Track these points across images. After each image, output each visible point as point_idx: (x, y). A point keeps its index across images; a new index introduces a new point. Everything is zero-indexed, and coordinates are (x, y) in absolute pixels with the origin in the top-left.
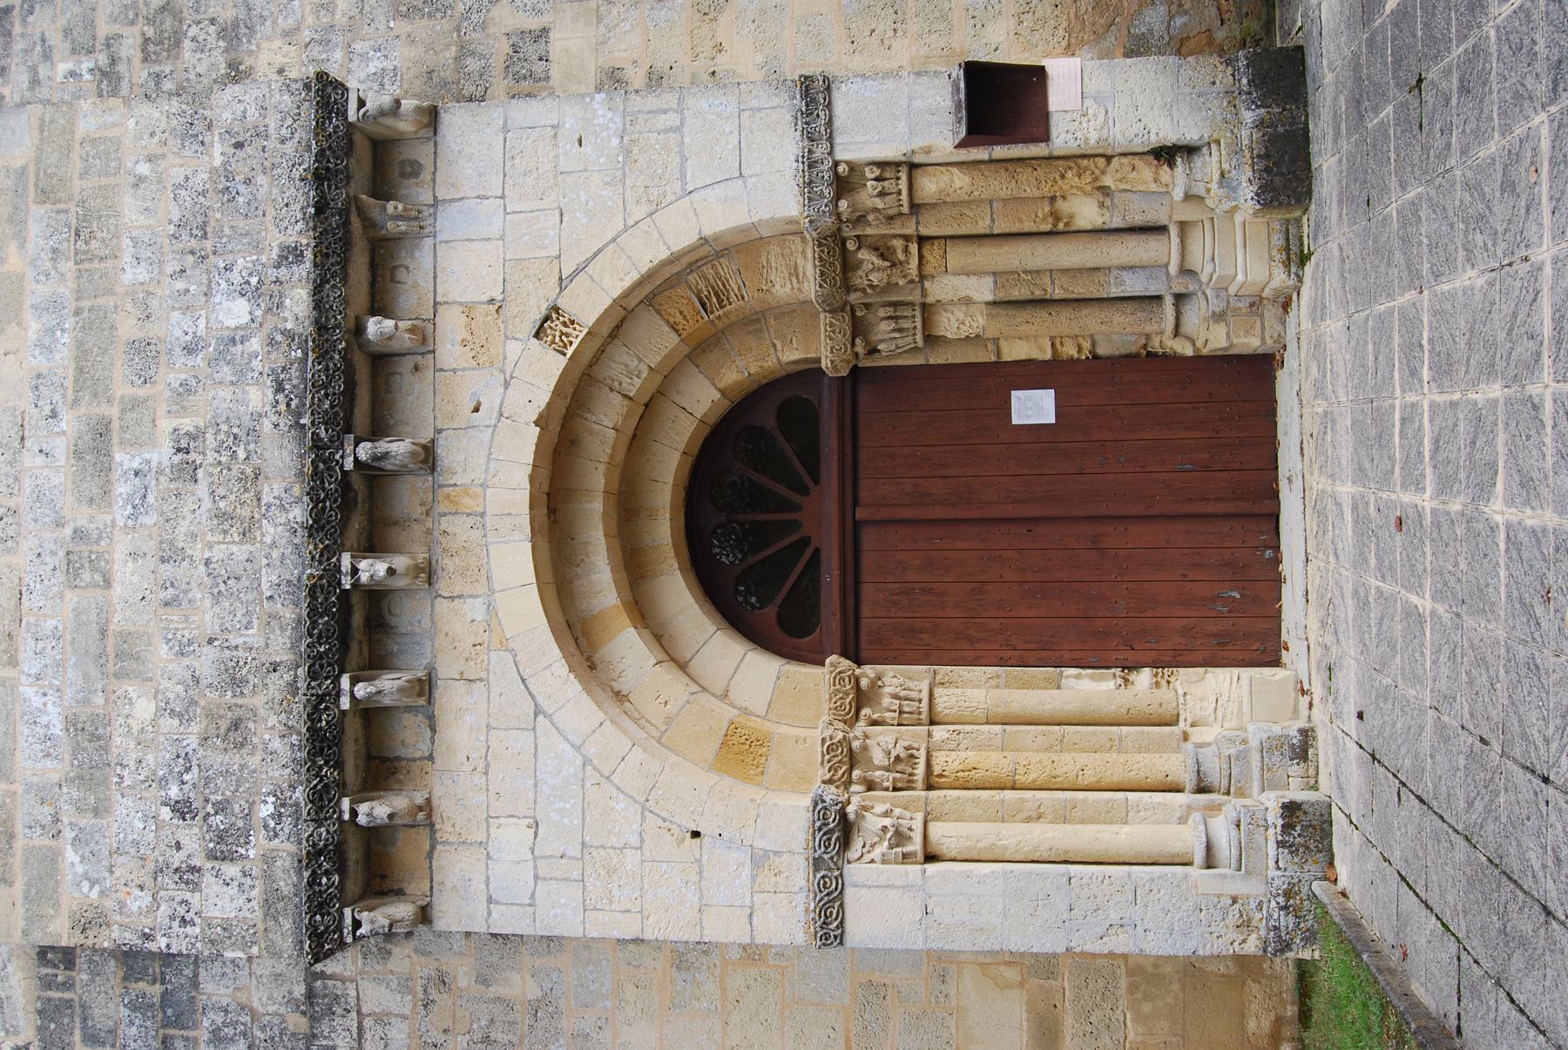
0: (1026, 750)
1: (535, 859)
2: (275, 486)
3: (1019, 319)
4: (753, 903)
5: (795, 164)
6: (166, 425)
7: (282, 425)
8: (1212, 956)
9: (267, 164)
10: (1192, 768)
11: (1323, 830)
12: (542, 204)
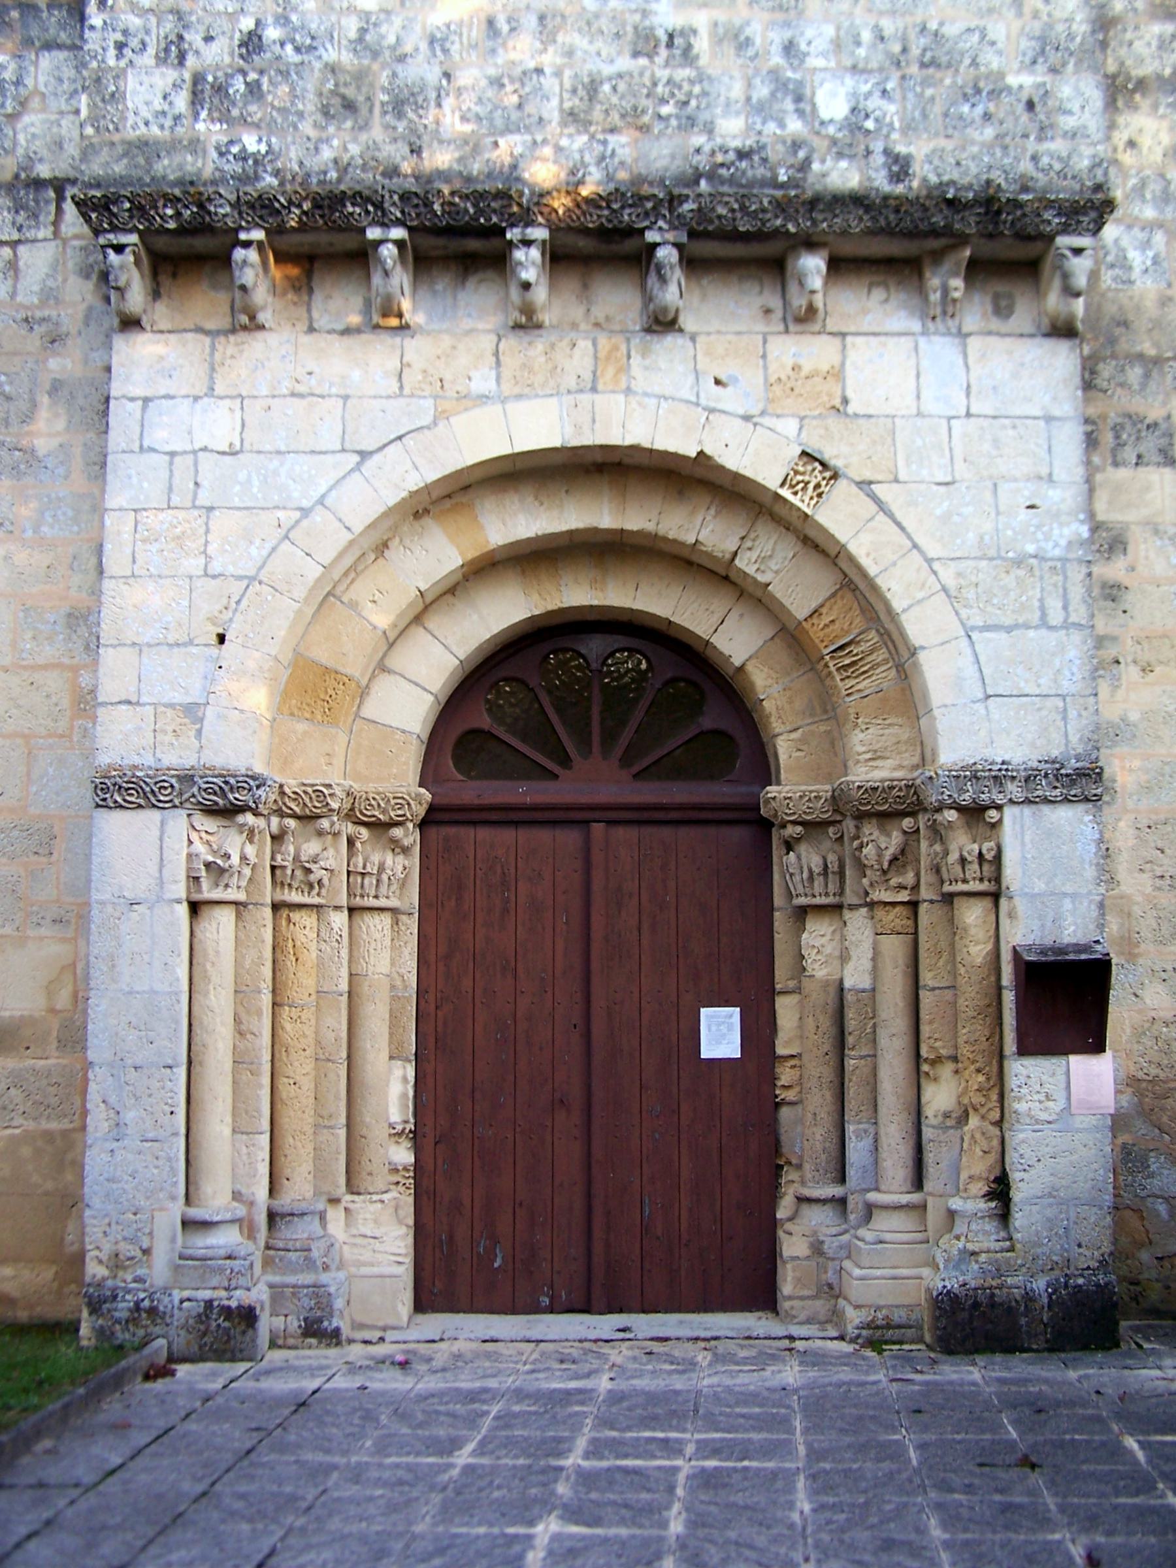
0: (317, 1020)
1: (194, 452)
2: (627, 150)
3: (821, 1019)
4: (144, 705)
5: (999, 760)
6: (701, 19)
7: (699, 158)
8: (83, 1226)
9: (1008, 140)
10: (298, 1207)
11: (224, 1351)
12: (960, 465)
